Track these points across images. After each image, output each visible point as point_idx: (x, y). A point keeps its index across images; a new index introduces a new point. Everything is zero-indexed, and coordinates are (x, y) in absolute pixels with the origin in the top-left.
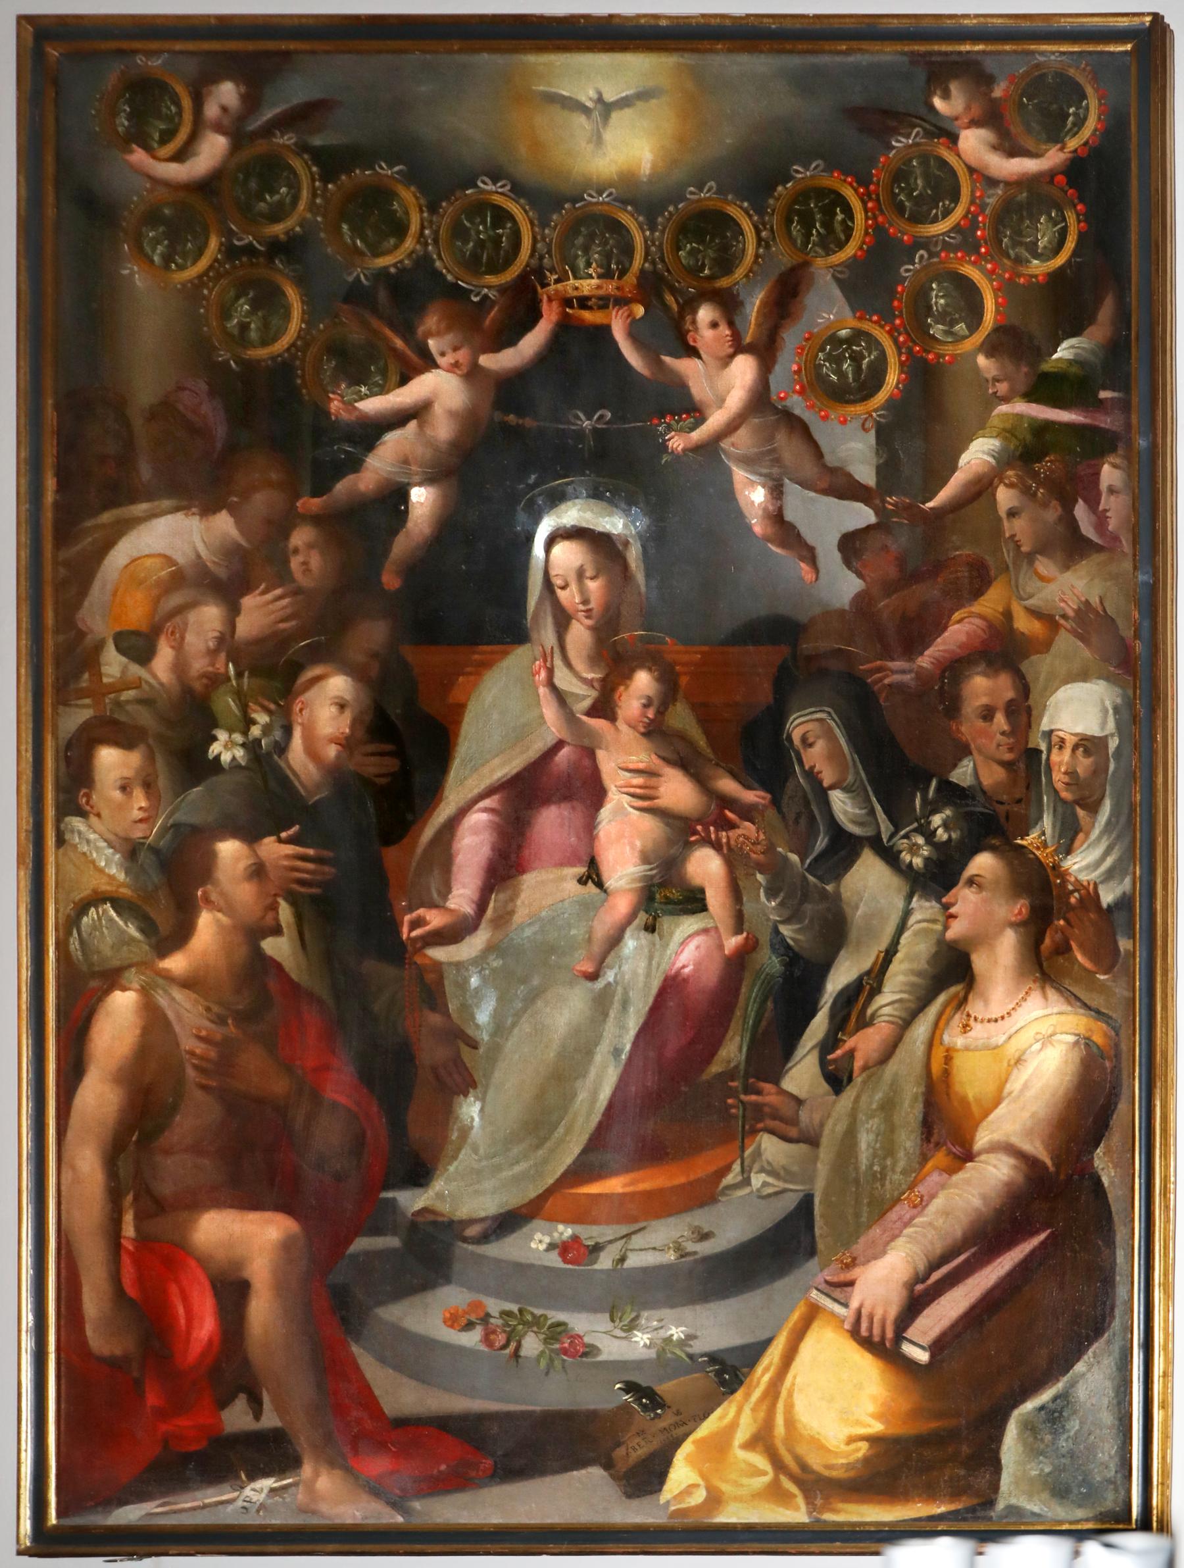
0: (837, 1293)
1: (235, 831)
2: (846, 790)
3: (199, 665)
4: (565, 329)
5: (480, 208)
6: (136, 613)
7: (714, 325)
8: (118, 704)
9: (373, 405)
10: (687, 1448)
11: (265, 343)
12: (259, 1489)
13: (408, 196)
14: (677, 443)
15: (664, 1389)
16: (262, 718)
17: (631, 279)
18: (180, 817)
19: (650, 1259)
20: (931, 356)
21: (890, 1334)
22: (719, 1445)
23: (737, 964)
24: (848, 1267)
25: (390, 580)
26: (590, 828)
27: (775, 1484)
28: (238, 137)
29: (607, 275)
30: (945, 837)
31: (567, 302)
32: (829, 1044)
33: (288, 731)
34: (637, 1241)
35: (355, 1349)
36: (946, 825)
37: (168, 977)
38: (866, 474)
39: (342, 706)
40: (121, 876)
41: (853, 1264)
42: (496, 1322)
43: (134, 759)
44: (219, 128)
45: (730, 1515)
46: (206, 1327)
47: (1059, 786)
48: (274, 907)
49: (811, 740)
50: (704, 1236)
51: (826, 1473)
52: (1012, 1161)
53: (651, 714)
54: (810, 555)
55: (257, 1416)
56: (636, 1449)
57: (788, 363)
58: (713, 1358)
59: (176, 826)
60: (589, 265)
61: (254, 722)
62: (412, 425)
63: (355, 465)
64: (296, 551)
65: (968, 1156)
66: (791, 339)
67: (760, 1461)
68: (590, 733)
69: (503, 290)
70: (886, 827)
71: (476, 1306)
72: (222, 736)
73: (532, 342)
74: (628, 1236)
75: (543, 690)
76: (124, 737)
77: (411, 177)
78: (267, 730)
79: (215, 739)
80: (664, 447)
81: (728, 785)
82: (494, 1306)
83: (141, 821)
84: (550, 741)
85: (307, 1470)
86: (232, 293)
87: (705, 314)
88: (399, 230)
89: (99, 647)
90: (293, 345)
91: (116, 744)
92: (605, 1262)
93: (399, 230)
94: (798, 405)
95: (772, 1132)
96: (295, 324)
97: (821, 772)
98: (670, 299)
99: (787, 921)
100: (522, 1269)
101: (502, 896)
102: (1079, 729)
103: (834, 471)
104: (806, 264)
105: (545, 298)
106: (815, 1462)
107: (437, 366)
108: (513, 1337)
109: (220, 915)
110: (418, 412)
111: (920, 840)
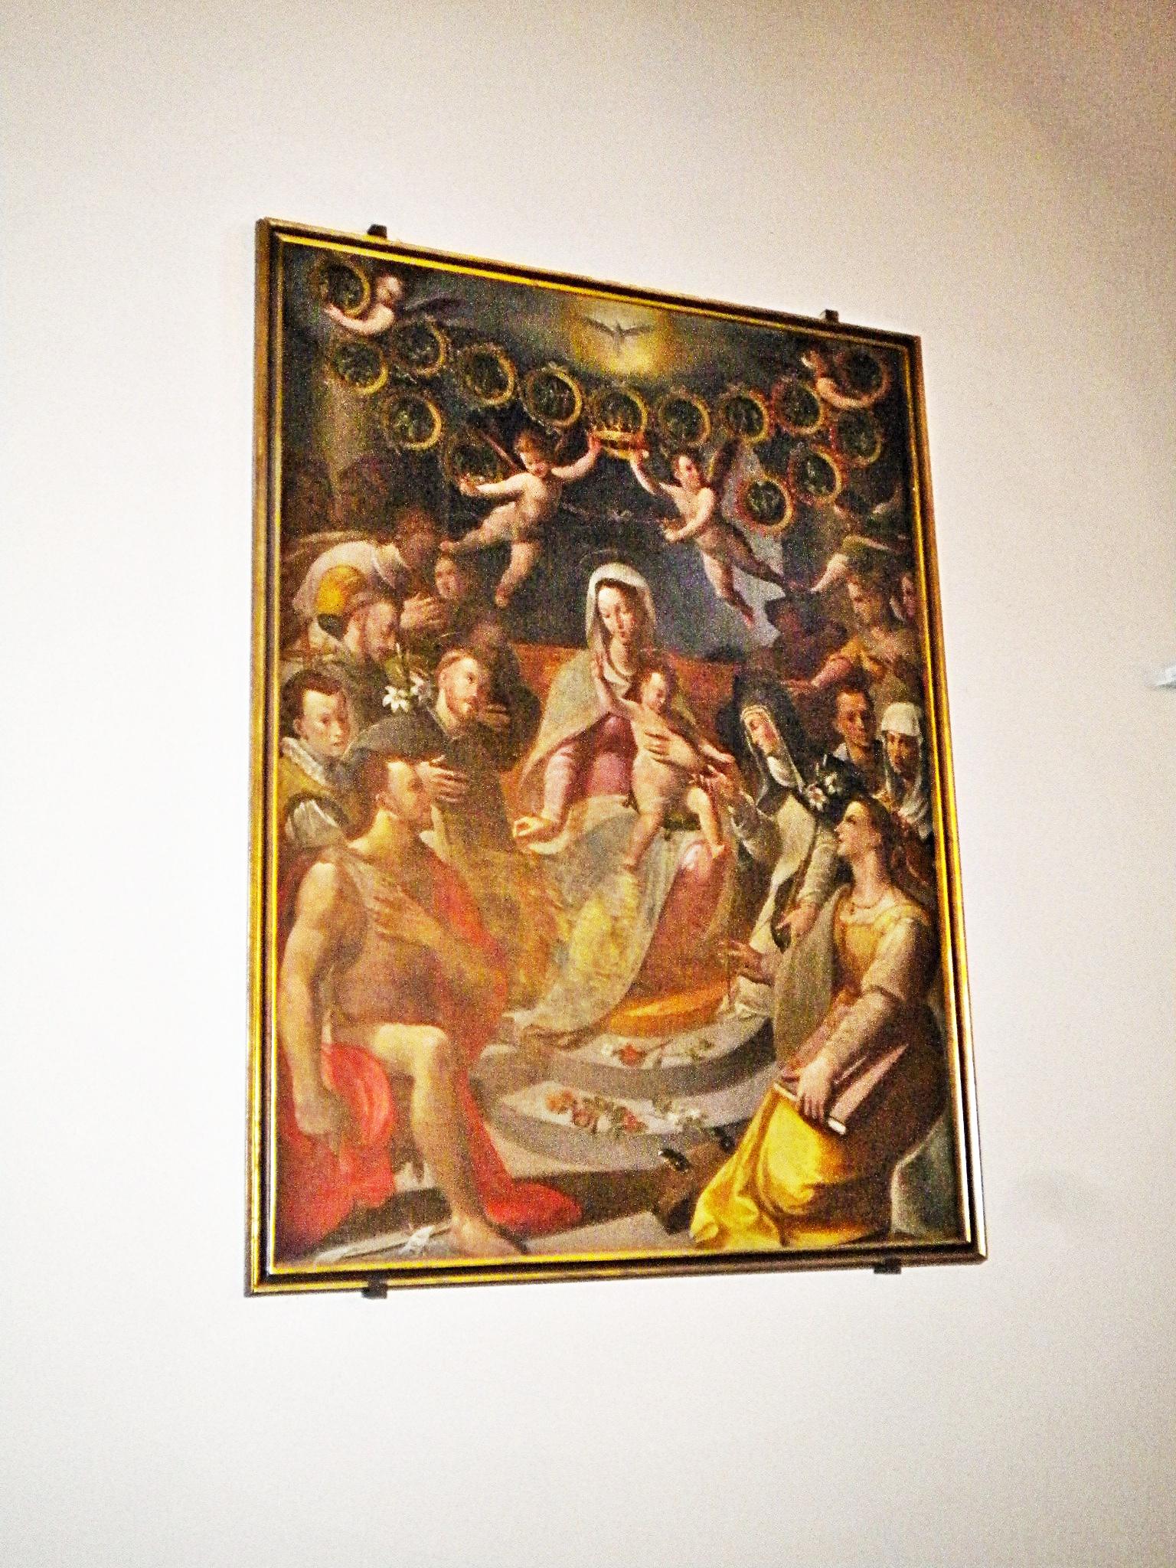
0: (790, 1086)
1: (402, 756)
2: (777, 757)
3: (376, 642)
4: (601, 457)
5: (550, 378)
6: (332, 601)
7: (689, 469)
8: (321, 663)
9: (489, 489)
10: (705, 1197)
11: (420, 438)
12: (420, 1236)
13: (506, 364)
14: (671, 535)
15: (688, 1153)
16: (419, 681)
17: (641, 435)
18: (363, 744)
19: (677, 1062)
20: (809, 503)
21: (822, 1112)
22: (724, 1193)
23: (719, 863)
24: (793, 1068)
25: (500, 600)
26: (629, 768)
27: (760, 1221)
28: (399, 311)
29: (625, 429)
30: (834, 791)
31: (603, 442)
32: (776, 918)
33: (436, 690)
34: (668, 1049)
35: (487, 1128)
36: (834, 783)
37: (355, 854)
38: (777, 569)
39: (471, 678)
40: (322, 782)
41: (799, 1064)
42: (581, 1106)
43: (332, 701)
44: (387, 304)
45: (730, 1247)
46: (383, 1110)
47: (893, 764)
48: (428, 810)
49: (756, 725)
50: (708, 1045)
51: (789, 1211)
52: (883, 998)
53: (662, 700)
54: (748, 611)
55: (420, 1177)
56: (672, 1197)
57: (731, 498)
58: (719, 1131)
59: (362, 750)
60: (615, 422)
61: (414, 684)
62: (512, 505)
63: (476, 525)
64: (440, 575)
65: (858, 994)
66: (731, 483)
67: (749, 1203)
68: (625, 709)
69: (565, 430)
70: (800, 781)
71: (567, 1096)
72: (391, 690)
73: (584, 463)
74: (662, 1046)
75: (597, 681)
76: (326, 686)
77: (509, 354)
78: (422, 689)
79: (387, 693)
80: (662, 538)
81: (709, 749)
82: (580, 1094)
83: (336, 744)
84: (603, 713)
85: (455, 1219)
86: (396, 407)
87: (683, 461)
88: (502, 386)
89: (307, 623)
90: (437, 444)
91: (320, 690)
92: (648, 1063)
93: (502, 386)
94: (739, 523)
95: (745, 975)
96: (437, 432)
97: (762, 746)
98: (662, 449)
99: (748, 838)
100: (598, 1068)
101: (575, 813)
102: (902, 732)
103: (760, 564)
104: (737, 442)
105: (590, 439)
106: (784, 1205)
107: (524, 469)
108: (592, 1118)
109: (391, 814)
110: (515, 497)
111: (819, 791)
